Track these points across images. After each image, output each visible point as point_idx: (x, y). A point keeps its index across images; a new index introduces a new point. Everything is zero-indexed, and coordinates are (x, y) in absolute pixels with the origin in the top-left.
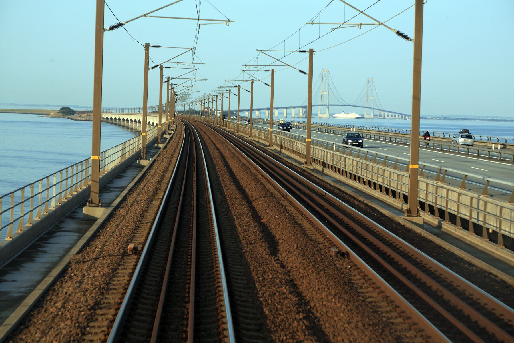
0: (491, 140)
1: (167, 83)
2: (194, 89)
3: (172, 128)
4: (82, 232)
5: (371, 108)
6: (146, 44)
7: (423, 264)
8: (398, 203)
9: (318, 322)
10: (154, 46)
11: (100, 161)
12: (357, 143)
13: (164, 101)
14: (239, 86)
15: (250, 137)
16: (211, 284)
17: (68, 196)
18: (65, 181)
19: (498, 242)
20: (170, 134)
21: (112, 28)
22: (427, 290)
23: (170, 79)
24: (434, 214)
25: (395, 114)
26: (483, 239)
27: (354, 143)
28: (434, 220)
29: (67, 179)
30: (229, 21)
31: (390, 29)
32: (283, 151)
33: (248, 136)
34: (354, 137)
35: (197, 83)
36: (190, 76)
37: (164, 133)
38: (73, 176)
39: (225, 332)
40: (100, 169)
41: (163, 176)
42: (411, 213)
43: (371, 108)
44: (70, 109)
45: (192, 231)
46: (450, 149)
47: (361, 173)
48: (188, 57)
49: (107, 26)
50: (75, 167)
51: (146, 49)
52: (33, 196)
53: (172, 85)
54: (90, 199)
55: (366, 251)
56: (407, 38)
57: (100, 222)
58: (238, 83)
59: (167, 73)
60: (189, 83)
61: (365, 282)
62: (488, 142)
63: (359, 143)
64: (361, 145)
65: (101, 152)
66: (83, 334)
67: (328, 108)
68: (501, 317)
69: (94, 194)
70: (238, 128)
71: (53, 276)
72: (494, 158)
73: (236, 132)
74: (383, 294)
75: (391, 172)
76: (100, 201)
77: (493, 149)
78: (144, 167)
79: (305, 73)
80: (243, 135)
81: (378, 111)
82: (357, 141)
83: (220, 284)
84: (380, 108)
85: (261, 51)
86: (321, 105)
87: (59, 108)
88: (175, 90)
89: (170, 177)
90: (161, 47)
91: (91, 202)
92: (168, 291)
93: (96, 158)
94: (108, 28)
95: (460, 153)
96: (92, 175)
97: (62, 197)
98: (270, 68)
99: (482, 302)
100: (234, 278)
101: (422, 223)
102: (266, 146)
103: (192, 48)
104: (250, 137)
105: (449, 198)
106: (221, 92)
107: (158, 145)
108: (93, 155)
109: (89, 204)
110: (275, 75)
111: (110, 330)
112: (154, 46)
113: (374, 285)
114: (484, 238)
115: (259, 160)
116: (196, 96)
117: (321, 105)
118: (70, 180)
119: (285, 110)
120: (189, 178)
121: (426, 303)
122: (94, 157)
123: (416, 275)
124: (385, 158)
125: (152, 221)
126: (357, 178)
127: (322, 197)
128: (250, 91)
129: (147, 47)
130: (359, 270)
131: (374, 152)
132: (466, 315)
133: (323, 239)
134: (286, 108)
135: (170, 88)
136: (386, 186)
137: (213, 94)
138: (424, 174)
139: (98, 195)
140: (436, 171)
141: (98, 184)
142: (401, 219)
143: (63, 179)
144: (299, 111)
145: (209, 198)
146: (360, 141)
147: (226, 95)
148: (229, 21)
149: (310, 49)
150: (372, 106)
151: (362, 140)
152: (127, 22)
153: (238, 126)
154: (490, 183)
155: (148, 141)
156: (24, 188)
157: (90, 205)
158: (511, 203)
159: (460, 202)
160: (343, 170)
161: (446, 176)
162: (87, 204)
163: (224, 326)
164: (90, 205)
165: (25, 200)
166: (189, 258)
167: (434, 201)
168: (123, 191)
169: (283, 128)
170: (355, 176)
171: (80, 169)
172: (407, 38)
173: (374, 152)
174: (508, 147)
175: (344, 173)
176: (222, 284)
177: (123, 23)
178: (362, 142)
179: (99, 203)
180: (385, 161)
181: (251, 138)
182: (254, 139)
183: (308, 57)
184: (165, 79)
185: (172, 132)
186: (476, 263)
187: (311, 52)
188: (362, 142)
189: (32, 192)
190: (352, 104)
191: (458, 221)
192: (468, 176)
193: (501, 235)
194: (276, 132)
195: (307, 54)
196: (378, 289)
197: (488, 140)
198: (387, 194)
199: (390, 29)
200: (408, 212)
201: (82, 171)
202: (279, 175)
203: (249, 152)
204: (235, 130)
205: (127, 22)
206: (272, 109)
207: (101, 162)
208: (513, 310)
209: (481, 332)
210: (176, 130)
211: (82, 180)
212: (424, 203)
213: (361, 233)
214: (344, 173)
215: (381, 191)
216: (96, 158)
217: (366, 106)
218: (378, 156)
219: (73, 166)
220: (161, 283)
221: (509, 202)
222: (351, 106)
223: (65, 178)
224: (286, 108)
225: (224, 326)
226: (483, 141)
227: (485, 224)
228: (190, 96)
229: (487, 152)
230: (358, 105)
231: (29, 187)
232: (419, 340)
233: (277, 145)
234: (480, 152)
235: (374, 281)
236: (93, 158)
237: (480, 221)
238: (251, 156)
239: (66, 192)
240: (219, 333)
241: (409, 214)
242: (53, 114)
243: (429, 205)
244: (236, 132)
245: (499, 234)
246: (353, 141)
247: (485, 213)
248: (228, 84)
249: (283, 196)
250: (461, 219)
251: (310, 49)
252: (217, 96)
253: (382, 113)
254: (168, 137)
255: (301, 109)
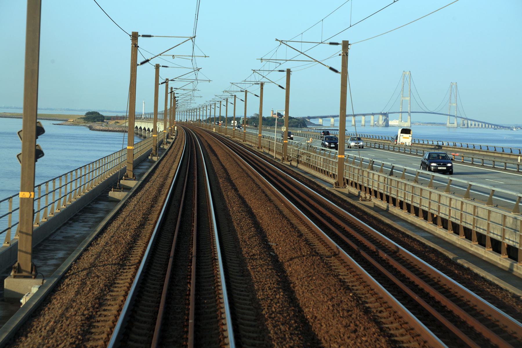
0: (456, 145)
1: (165, 84)
2: (196, 93)
3: (174, 134)
4: (72, 250)
5: (454, 116)
6: (133, 32)
7: (478, 311)
8: (332, 181)
9: (294, 287)
10: (143, 36)
11: (34, 200)
12: (445, 168)
13: (169, 107)
14: (235, 96)
15: (244, 141)
16: (213, 309)
17: (49, 216)
18: (45, 197)
19: (502, 253)
20: (172, 139)
21: (142, 63)
22: (441, 309)
23: (173, 90)
24: (458, 234)
25: (479, 123)
26: (460, 237)
27: (440, 168)
28: (383, 205)
29: (61, 188)
30: (210, 81)
31: (325, 66)
32: (301, 166)
33: (242, 141)
34: (439, 159)
35: (200, 86)
36: (192, 76)
37: (161, 143)
38: (77, 179)
39: (225, 333)
40: (34, 213)
41: (90, 318)
42: (338, 185)
43: (454, 116)
44: (99, 114)
45: (191, 265)
46: (494, 165)
47: (397, 193)
48: (186, 49)
49: (139, 62)
50: (79, 171)
51: (132, 38)
52: (11, 211)
53: (172, 88)
54: (126, 174)
55: (369, 261)
56: (283, 88)
57: (167, 150)
58: (245, 87)
59: (171, 84)
60: (190, 86)
61: (399, 327)
62: (454, 147)
63: (447, 167)
64: (449, 171)
65: (36, 185)
66: (83, 340)
67: (410, 115)
68: (489, 318)
69: (24, 254)
70: (234, 134)
71: (55, 277)
72: (510, 170)
73: (232, 137)
74: (376, 296)
75: (398, 182)
76: (34, 267)
77: (519, 161)
78: (155, 162)
79: (258, 96)
80: (238, 140)
81: (461, 119)
82: (444, 165)
83: (219, 284)
84: (464, 116)
85: (282, 41)
86: (402, 112)
87: (83, 114)
88: (176, 95)
89: (171, 182)
90: (153, 36)
91: (19, 270)
92: (190, 160)
93: (27, 195)
94: (139, 64)
95: (485, 166)
96: (21, 222)
97: (67, 201)
98: (285, 67)
99: (479, 308)
100: (235, 289)
101: (373, 206)
102: (279, 160)
103: (192, 37)
104: (244, 141)
105: (464, 210)
106: (225, 97)
107: (152, 158)
108: (22, 190)
109: (15, 272)
110: (291, 76)
111: (106, 343)
112: (143, 36)
113: (364, 284)
114: (420, 217)
115: (277, 180)
116: (197, 103)
117: (402, 112)
118: (74, 183)
119: (363, 118)
120: (184, 233)
121: (412, 300)
122: (23, 193)
123: (344, 228)
124: (491, 192)
125: (131, 277)
126: (358, 186)
127: (394, 254)
128: (259, 95)
129: (135, 36)
130: (369, 287)
131: (465, 182)
132: (486, 338)
133: (345, 269)
134: (364, 115)
135: (169, 91)
136: (416, 205)
137: (217, 100)
138: (384, 171)
139: (29, 257)
140: (414, 173)
141: (132, 165)
142: (334, 190)
143: (73, 179)
144: (379, 119)
145: (205, 177)
146: (449, 165)
147: (231, 100)
148: (210, 81)
149: (344, 41)
150: (456, 113)
151: (451, 163)
152: (152, 58)
153: (234, 132)
154: (364, 160)
155: (41, 219)
156: (55, 179)
157: (17, 274)
158: (466, 198)
159: (476, 215)
160: (352, 182)
161: (405, 174)
162: (12, 273)
163: (223, 321)
164: (17, 274)
165: (13, 211)
166: (188, 275)
167: (447, 213)
168: (71, 254)
169: (330, 143)
170: (375, 192)
171: (57, 185)
172: (283, 88)
173: (465, 182)
174: (443, 148)
175: (354, 184)
176: (226, 321)
177: (149, 59)
178: (451, 167)
179: (32, 271)
180: (468, 192)
181: (244, 142)
182: (248, 143)
183: (286, 77)
184: (169, 91)
185: (174, 137)
186: (504, 286)
187: (346, 45)
188: (451, 167)
189: (11, 206)
190: (434, 112)
191: (488, 243)
192: (495, 192)
193: (475, 233)
194: (279, 140)
195: (285, 73)
196: (385, 304)
197: (454, 145)
198: (402, 208)
199: (325, 66)
200: (336, 185)
201: (61, 188)
202: (286, 188)
203: (277, 180)
204: (231, 135)
205: (152, 58)
206: (343, 115)
207: (36, 203)
208: (521, 324)
209: (477, 337)
210: (177, 135)
211: (76, 189)
212: (427, 212)
213: (358, 238)
214: (354, 184)
215: (382, 199)
216: (27, 195)
217: (449, 114)
218: (406, 171)
219: (77, 169)
220: (159, 299)
221: (429, 187)
222: (434, 113)
223: (59, 187)
224: (364, 115)
225: (224, 327)
226: (463, 148)
227: (429, 210)
228: (192, 101)
229: (471, 159)
230: (440, 113)
231: (7, 201)
232: (414, 344)
233: (267, 148)
234: (485, 161)
235: (365, 279)
236: (22, 195)
237: (506, 238)
238: (250, 161)
239: (89, 184)
240: (218, 334)
241: (337, 186)
242: (72, 120)
243: (415, 207)
244: (232, 137)
245: (519, 250)
246: (439, 165)
247: (489, 222)
248: (234, 88)
249: (234, 155)
250: (492, 240)
251: (344, 41)
252: (221, 102)
253: (465, 122)
254: (166, 147)
255: (381, 117)
